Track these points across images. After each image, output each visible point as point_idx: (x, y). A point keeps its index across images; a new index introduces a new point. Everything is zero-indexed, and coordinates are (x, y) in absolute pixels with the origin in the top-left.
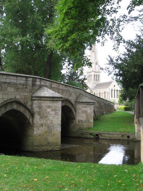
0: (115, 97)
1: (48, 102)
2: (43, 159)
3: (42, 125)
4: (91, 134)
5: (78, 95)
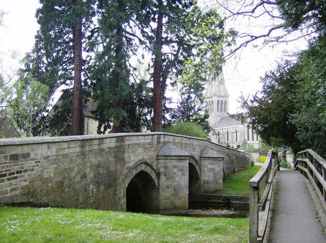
0: (253, 140)
1: (174, 161)
2: (141, 214)
3: (168, 187)
4: (219, 198)
5: (203, 148)
